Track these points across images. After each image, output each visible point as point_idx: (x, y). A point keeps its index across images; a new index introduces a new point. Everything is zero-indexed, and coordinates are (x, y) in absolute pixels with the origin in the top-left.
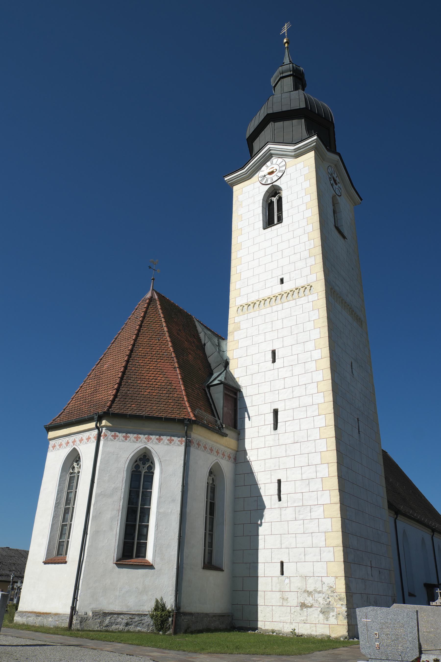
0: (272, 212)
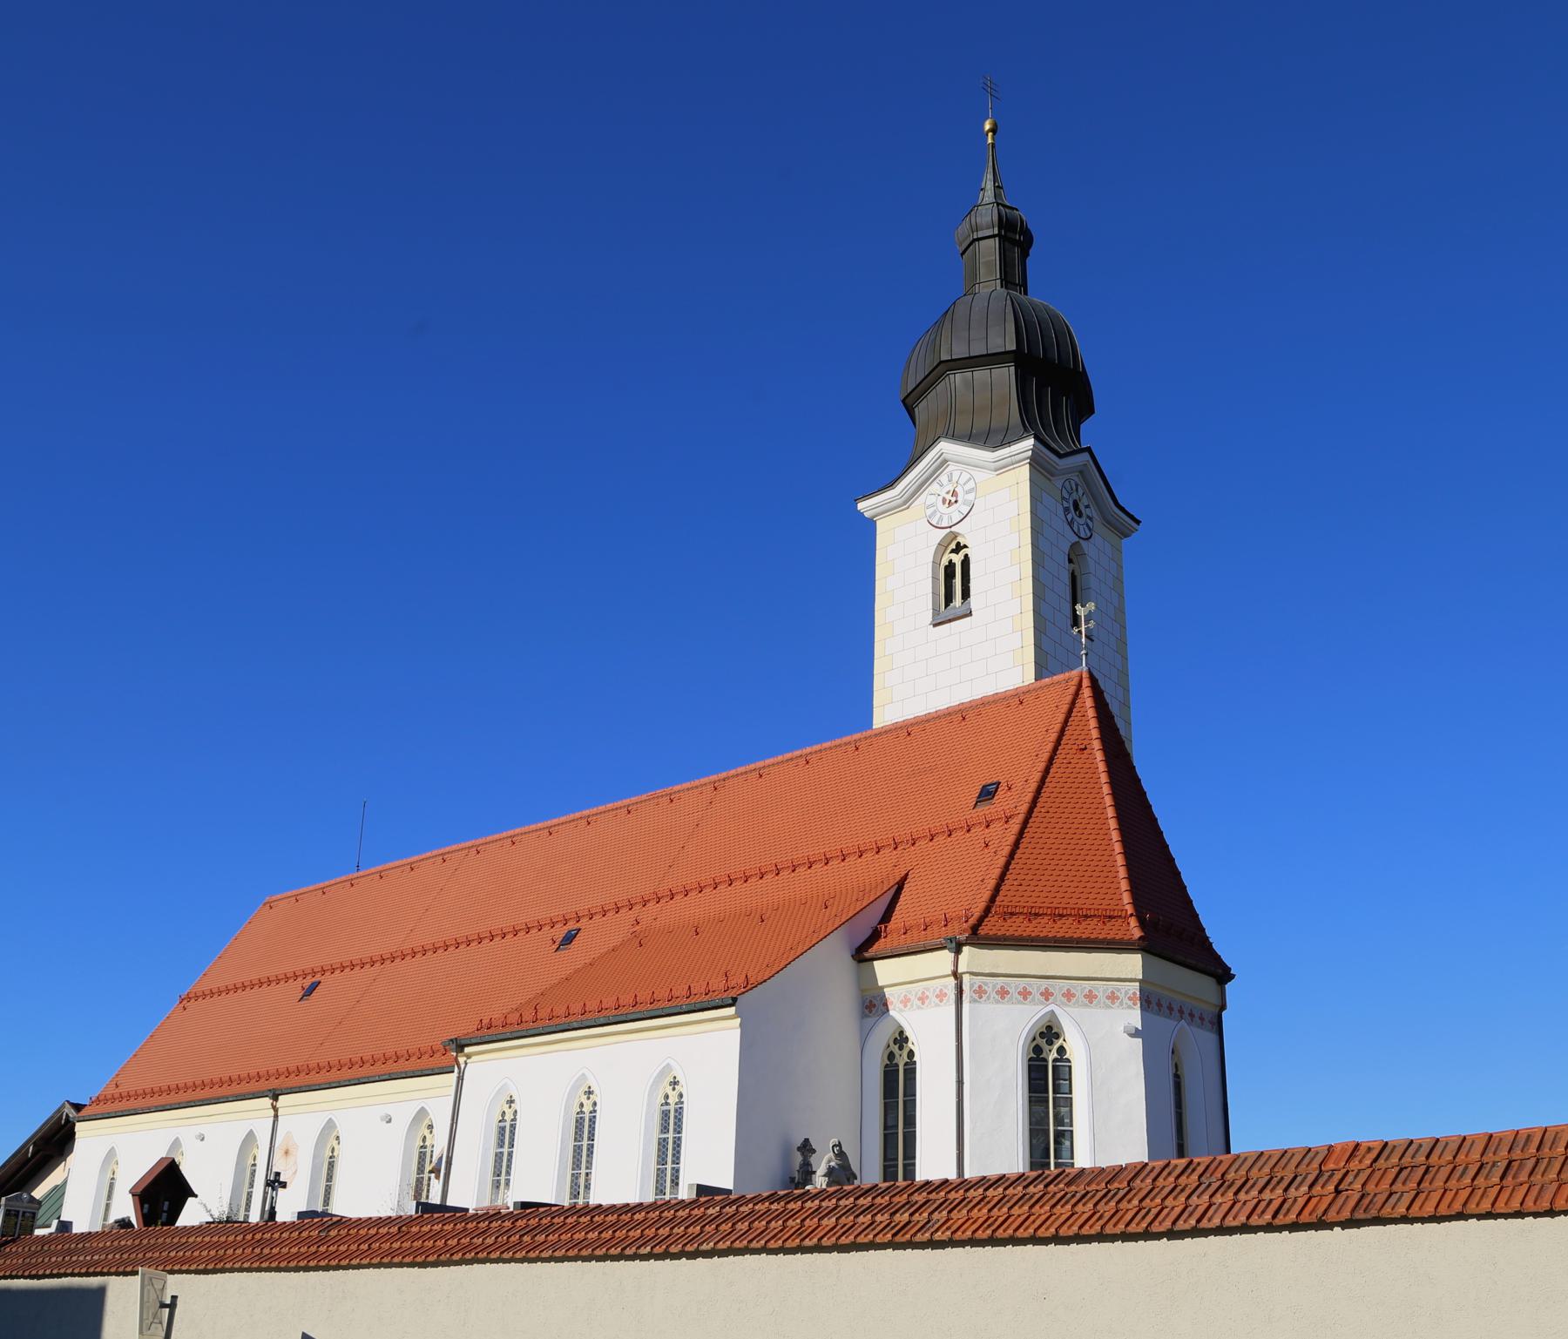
0: (954, 583)
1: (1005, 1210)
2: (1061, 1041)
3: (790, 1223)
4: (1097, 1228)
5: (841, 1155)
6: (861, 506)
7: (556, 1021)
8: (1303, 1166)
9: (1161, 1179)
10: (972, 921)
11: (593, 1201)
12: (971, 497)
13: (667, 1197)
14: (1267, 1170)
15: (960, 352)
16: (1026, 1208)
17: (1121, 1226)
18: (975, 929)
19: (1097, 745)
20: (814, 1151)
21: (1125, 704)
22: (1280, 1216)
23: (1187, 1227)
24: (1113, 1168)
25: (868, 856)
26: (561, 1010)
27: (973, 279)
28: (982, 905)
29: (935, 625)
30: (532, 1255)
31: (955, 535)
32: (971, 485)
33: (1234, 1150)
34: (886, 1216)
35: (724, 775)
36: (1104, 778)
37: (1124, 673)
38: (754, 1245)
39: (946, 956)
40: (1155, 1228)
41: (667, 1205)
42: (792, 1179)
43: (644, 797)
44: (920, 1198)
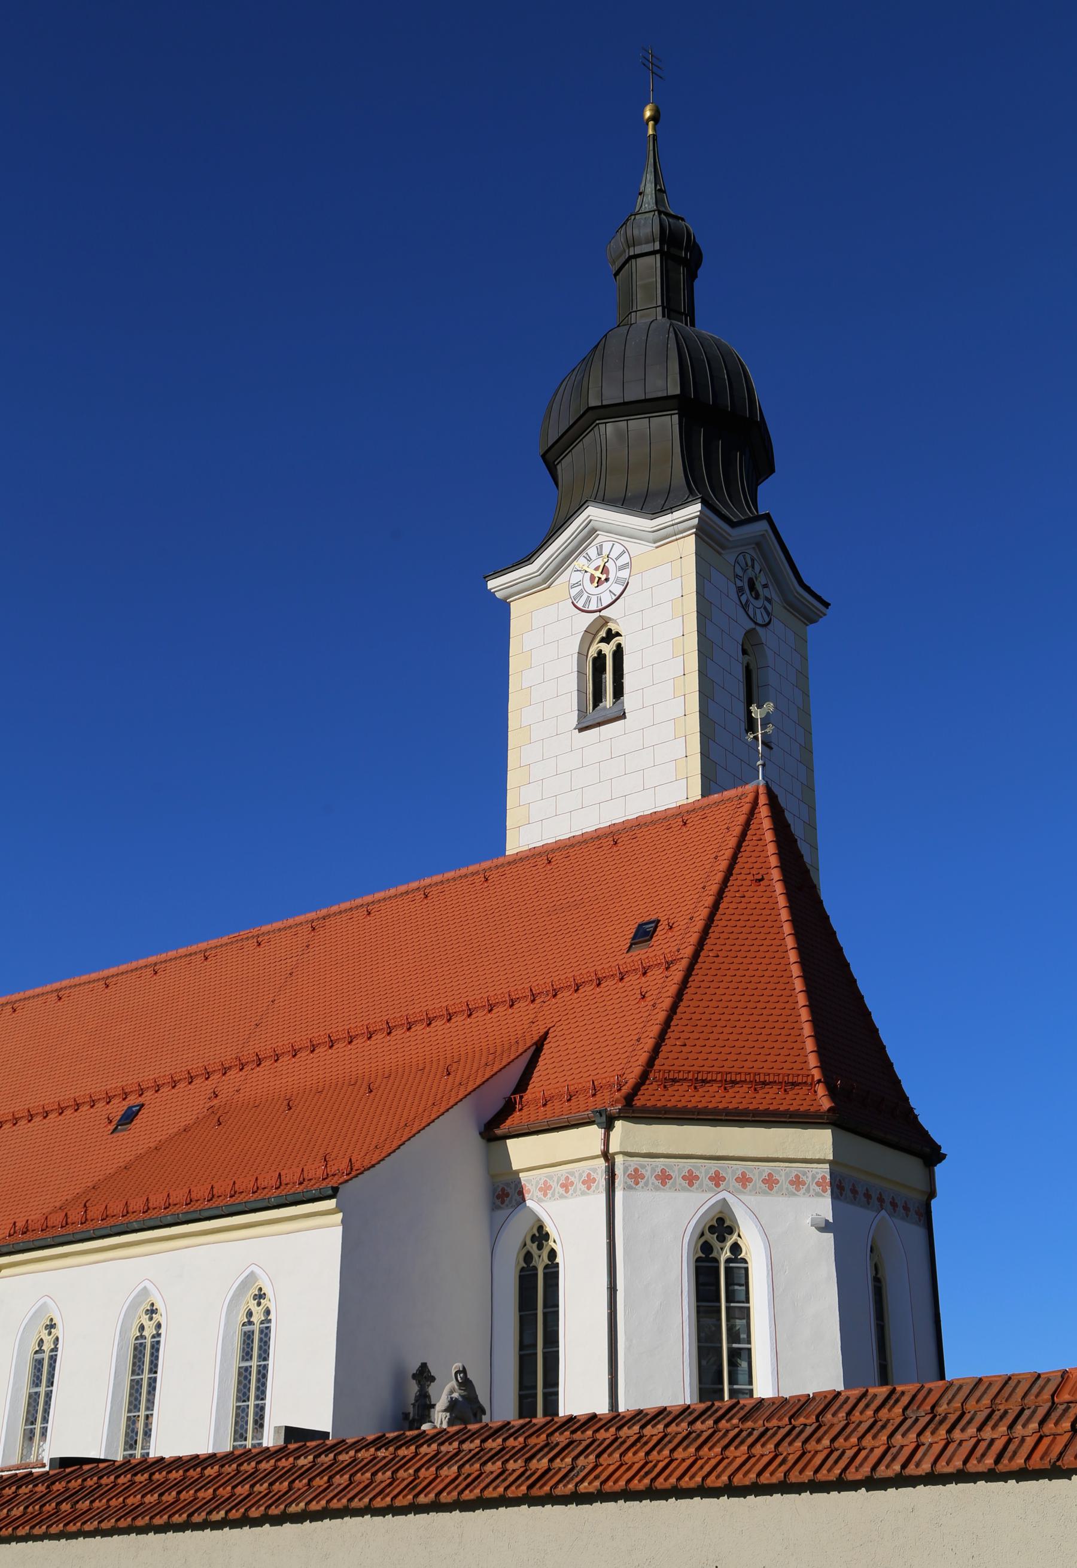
0: (603, 681)
1: (666, 1452)
2: (735, 1237)
3: (401, 1474)
4: (779, 1475)
5: (466, 1384)
6: (491, 584)
7: (111, 1222)
8: (1031, 1397)
9: (857, 1413)
10: (626, 1089)
11: (154, 1453)
12: (624, 574)
13: (249, 1444)
14: (986, 1401)
15: (612, 395)
16: (692, 1450)
17: (809, 1473)
18: (629, 1099)
19: (776, 874)
20: (433, 1379)
21: (811, 826)
22: (1005, 1461)
23: (890, 1473)
24: (798, 1398)
25: (499, 1010)
26: (117, 1208)
27: (628, 305)
28: (637, 1071)
29: (581, 730)
30: (72, 1528)
31: (605, 621)
32: (625, 559)
33: (948, 1378)
34: (520, 1462)
35: (324, 912)
36: (785, 915)
37: (809, 787)
38: (356, 1504)
39: (595, 1133)
40: (851, 1475)
41: (246, 1456)
42: (406, 1415)
43: (225, 940)
44: (561, 1438)
